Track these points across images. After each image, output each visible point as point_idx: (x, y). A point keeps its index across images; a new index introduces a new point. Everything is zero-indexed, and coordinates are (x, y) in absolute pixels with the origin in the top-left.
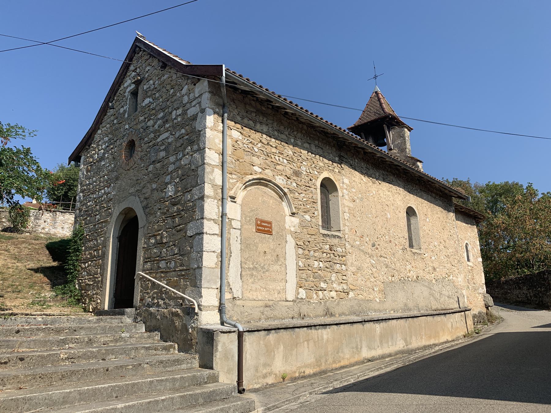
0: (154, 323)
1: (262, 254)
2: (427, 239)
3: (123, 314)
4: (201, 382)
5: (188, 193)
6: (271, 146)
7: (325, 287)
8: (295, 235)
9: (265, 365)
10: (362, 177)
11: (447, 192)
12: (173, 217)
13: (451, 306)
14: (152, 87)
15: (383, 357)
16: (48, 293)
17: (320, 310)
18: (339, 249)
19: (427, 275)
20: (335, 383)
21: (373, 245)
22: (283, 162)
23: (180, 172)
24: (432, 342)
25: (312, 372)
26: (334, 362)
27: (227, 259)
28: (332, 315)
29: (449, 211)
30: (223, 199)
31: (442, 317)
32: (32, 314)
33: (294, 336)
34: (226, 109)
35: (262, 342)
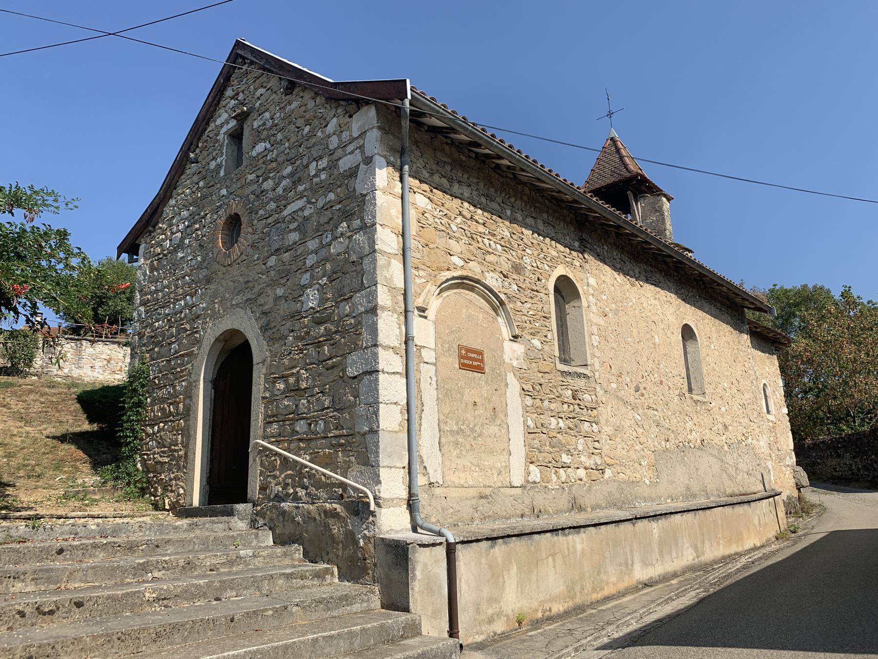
0: (289, 529)
1: (470, 406)
2: (713, 378)
3: (230, 513)
4: (394, 636)
5: (344, 303)
6: (477, 222)
7: (568, 461)
9: (492, 600)
10: (616, 274)
11: (738, 300)
12: (319, 345)
13: (754, 489)
14: (269, 123)
15: (665, 578)
16: (89, 478)
17: (563, 502)
18: (587, 397)
19: (705, 439)
20: (609, 629)
21: (637, 390)
22: (495, 249)
23: (328, 266)
24: (734, 549)
25: (562, 609)
26: (594, 590)
27: (417, 416)
28: (581, 509)
29: (741, 332)
30: (406, 311)
31: (746, 506)
32: (69, 515)
33: (533, 549)
34: (407, 158)
35: (483, 561)
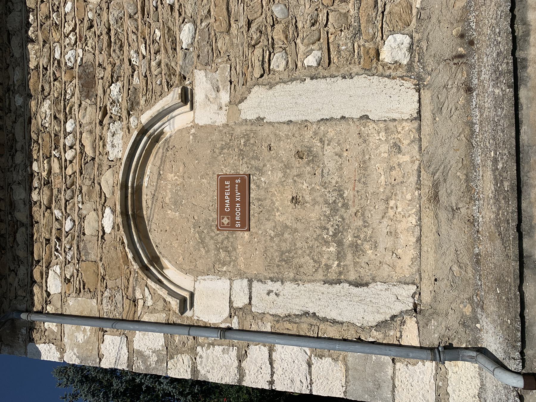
1: (298, 211)
8: (240, 86)
